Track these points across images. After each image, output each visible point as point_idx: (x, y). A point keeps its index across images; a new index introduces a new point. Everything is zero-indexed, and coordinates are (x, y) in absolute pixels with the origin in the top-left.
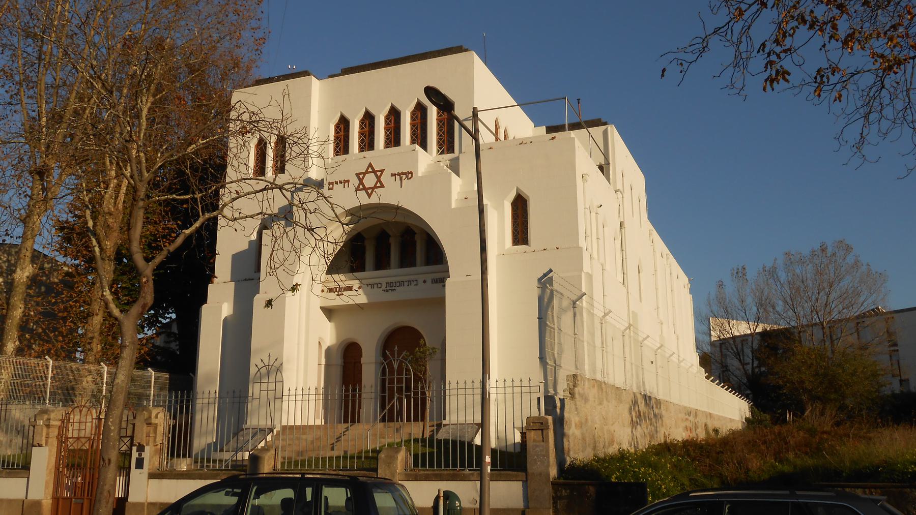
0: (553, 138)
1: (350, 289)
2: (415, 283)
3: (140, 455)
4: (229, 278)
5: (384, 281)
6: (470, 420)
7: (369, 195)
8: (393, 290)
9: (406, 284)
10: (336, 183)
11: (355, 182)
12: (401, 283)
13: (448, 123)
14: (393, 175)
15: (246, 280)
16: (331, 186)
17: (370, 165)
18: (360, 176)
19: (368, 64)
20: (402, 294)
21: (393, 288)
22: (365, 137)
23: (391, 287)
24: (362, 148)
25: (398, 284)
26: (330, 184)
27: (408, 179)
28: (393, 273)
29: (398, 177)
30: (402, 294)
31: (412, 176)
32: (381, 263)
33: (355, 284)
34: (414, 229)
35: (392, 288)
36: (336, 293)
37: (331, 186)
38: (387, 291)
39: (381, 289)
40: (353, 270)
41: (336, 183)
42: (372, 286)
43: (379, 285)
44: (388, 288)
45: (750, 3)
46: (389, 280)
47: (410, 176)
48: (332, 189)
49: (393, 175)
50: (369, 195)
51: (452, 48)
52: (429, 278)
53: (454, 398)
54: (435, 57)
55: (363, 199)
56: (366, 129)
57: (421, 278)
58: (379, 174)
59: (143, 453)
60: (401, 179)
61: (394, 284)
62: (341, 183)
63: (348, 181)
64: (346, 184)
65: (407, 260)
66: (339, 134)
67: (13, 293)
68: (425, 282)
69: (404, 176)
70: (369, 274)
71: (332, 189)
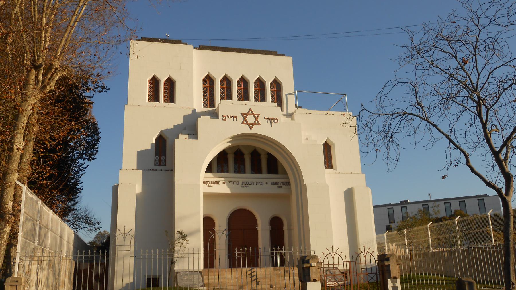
0: (433, 122)
1: (217, 183)
2: (261, 183)
3: (394, 284)
4: (135, 167)
5: (240, 181)
6: (196, 268)
7: (251, 128)
8: (247, 187)
9: (255, 183)
10: (228, 117)
11: (240, 119)
12: (252, 183)
13: (277, 94)
14: (265, 118)
15: (151, 170)
16: (224, 118)
17: (250, 110)
18: (244, 116)
19: (218, 47)
20: (252, 189)
21: (247, 185)
22: (224, 90)
23: (245, 184)
24: (222, 97)
25: (250, 183)
26: (223, 116)
27: (275, 122)
28: (248, 176)
29: (269, 121)
30: (252, 189)
31: (278, 121)
32: (240, 169)
33: (221, 180)
34: (260, 151)
35: (246, 185)
36: (208, 185)
37: (224, 118)
38: (243, 187)
39: (239, 185)
40: (222, 171)
41: (228, 117)
42: (233, 182)
43: (237, 183)
44: (243, 185)
45: (471, 77)
46: (244, 180)
47: (276, 121)
48: (225, 120)
49: (265, 118)
50: (251, 128)
51: (271, 51)
52: (270, 181)
53: (71, 255)
54: (260, 54)
55: (245, 130)
56: (225, 86)
57: (264, 181)
58: (256, 116)
59: (396, 283)
60: (271, 122)
61: (247, 183)
62: (232, 117)
63: (236, 117)
64: (235, 119)
65: (256, 169)
66: (205, 86)
67: (12, 161)
68: (267, 183)
69: (273, 121)
70: (231, 175)
71: (225, 120)
